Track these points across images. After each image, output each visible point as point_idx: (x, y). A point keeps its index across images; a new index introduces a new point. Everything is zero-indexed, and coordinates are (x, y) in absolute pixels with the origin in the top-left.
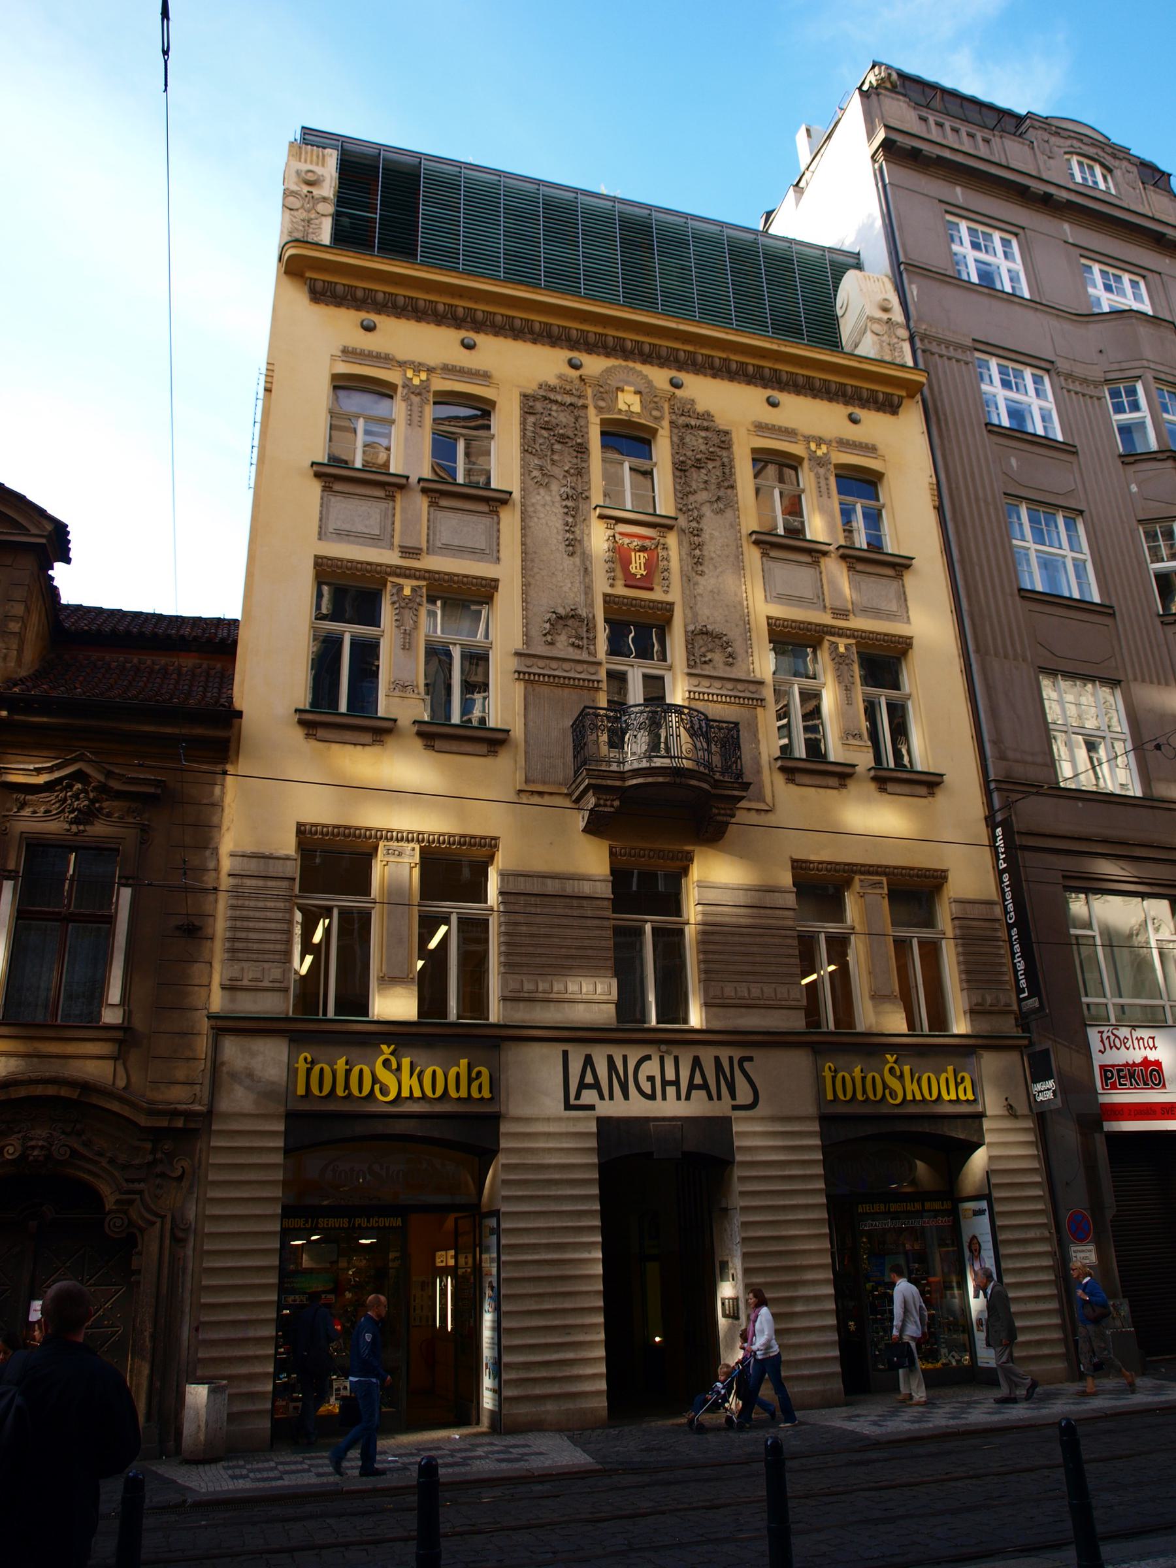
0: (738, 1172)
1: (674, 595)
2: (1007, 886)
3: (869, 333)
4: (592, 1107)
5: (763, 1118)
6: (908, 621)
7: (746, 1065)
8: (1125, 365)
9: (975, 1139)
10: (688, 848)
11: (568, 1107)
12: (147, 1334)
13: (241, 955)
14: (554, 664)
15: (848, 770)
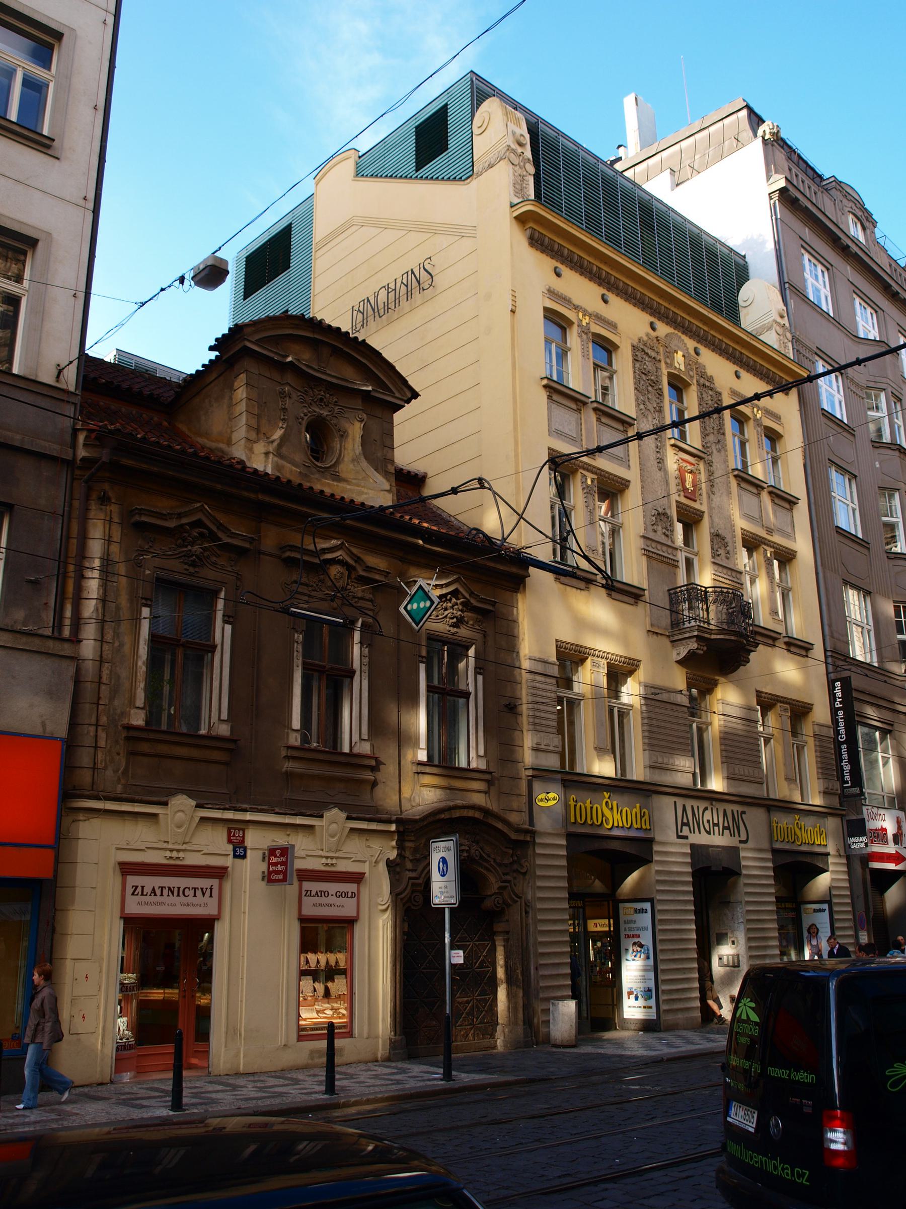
0: (743, 880)
1: (704, 508)
2: (841, 719)
3: (773, 331)
4: (686, 837)
5: (751, 849)
6: (795, 541)
7: (743, 815)
8: (878, 379)
9: (826, 868)
10: (717, 678)
11: (679, 837)
12: (519, 971)
13: (538, 728)
14: (659, 547)
15: (810, 646)
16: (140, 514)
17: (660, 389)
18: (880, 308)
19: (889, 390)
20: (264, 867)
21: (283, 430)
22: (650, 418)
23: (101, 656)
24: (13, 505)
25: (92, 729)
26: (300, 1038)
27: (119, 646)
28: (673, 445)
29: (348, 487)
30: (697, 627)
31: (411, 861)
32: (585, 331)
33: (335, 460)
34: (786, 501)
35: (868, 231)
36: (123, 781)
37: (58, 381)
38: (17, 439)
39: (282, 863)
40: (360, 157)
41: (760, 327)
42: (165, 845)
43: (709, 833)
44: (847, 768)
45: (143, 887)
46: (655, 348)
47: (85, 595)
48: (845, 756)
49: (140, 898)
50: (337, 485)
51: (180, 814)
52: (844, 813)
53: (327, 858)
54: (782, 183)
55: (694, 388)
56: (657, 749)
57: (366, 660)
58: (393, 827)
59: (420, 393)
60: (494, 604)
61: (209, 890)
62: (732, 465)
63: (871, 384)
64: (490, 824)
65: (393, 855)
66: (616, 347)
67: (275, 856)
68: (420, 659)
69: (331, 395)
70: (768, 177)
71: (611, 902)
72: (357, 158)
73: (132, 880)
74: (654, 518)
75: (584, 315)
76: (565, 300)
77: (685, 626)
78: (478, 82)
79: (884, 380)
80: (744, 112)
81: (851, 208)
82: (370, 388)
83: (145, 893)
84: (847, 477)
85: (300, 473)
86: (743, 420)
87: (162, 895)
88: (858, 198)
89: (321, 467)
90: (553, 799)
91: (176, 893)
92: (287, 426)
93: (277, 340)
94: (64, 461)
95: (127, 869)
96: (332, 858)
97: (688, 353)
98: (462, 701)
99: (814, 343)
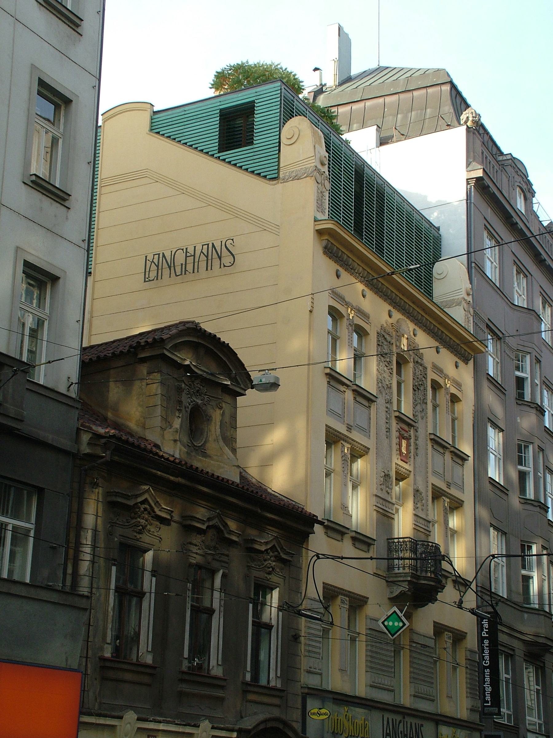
3: (461, 308)
8: (526, 344)
16: (116, 496)
18: (530, 273)
21: (180, 419)
22: (384, 395)
29: (212, 462)
30: (410, 574)
34: (461, 458)
37: (68, 390)
38: (50, 438)
40: (155, 113)
41: (450, 301)
44: (489, 689)
46: (390, 333)
48: (488, 679)
50: (205, 461)
54: (480, 173)
55: (411, 365)
57: (223, 603)
70: (468, 165)
72: (152, 112)
74: (382, 479)
75: (351, 310)
78: (285, 91)
79: (530, 345)
80: (447, 88)
84: (497, 430)
86: (436, 388)
89: (197, 446)
92: (182, 415)
97: (410, 335)
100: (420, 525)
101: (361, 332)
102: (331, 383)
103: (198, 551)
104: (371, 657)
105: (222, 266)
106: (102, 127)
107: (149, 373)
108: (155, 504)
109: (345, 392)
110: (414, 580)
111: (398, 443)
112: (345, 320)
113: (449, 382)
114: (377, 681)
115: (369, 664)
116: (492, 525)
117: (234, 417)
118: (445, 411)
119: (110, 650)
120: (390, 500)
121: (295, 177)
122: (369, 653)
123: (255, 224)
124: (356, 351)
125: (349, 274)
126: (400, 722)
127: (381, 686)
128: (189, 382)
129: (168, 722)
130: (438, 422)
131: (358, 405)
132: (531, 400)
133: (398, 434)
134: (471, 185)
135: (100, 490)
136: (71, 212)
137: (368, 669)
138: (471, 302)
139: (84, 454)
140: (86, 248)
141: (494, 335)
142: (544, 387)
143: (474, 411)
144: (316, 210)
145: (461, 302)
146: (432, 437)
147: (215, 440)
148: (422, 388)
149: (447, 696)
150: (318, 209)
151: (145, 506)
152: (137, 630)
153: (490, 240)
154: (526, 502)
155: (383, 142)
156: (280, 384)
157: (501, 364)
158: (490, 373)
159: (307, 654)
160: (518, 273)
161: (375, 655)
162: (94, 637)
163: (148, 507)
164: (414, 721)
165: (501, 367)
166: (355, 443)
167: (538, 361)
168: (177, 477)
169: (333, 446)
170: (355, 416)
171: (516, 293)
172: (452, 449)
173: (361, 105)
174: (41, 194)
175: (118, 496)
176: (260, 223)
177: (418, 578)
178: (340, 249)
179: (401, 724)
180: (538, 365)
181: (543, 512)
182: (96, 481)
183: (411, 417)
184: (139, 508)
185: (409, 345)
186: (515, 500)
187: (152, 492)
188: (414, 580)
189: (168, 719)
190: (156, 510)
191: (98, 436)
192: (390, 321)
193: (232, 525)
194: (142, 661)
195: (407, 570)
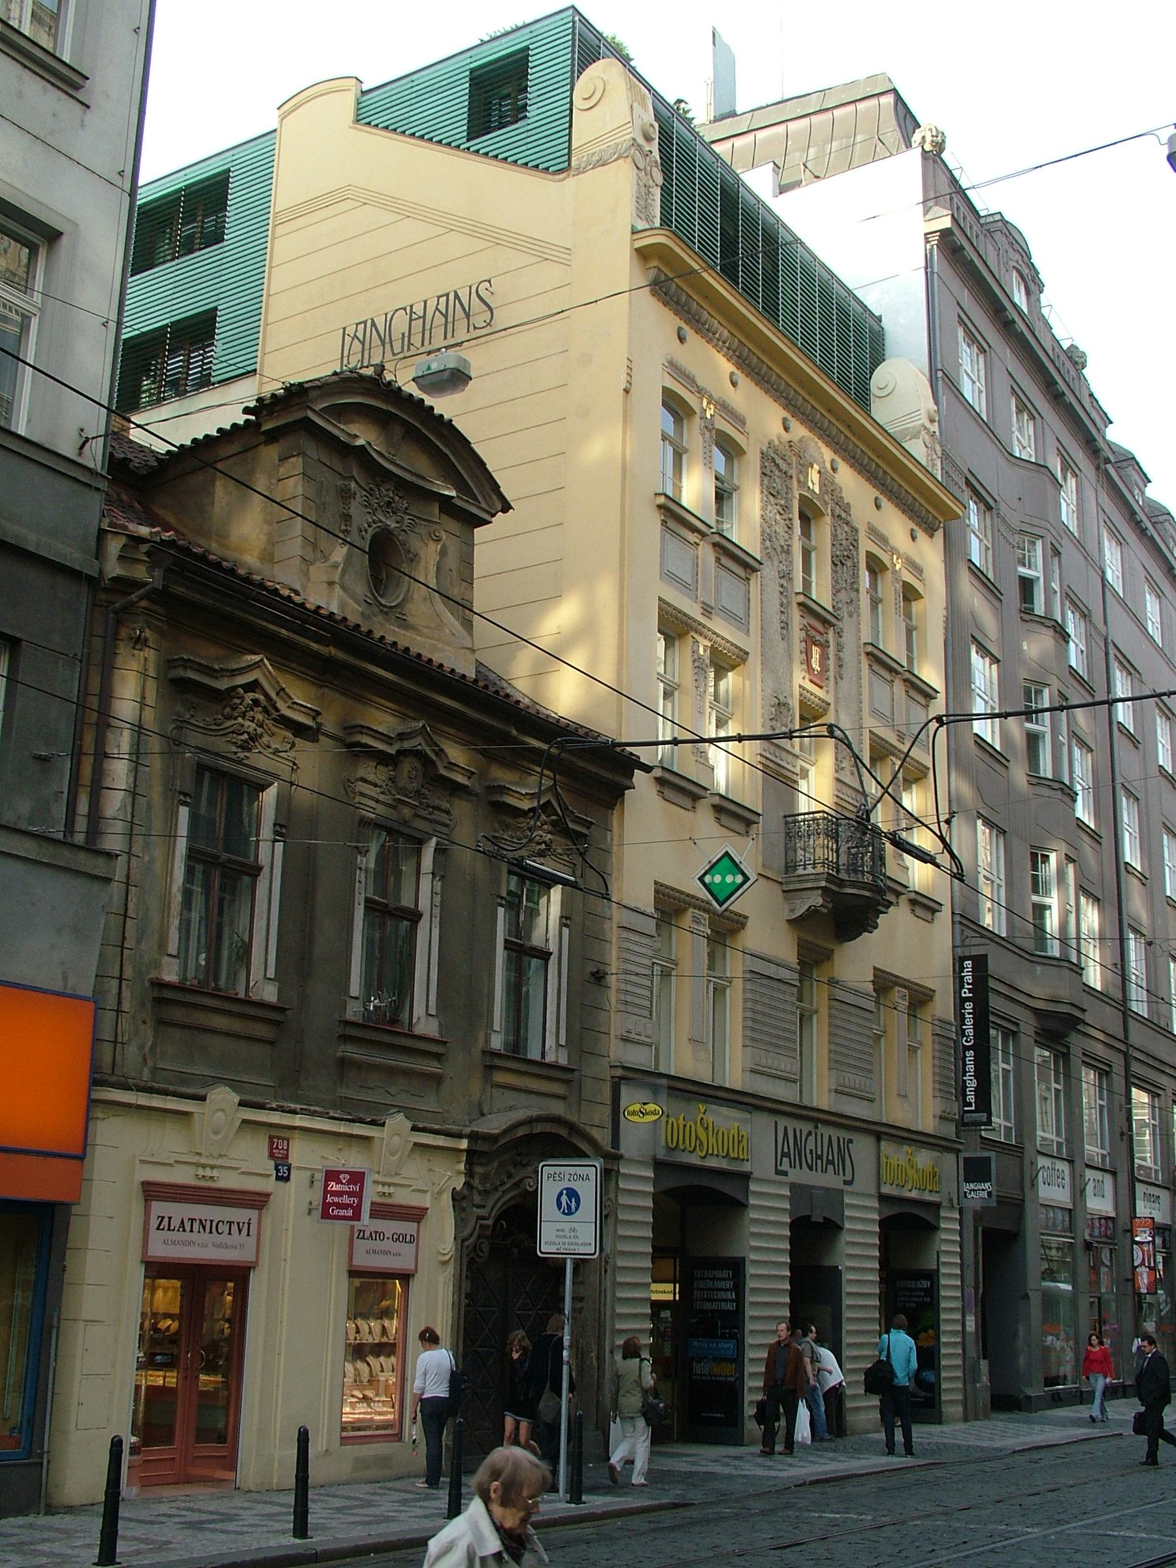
0: (845, 1237)
2: (969, 1013)
3: (920, 442)
4: (785, 1173)
8: (1035, 521)
15: (936, 906)
16: (185, 668)
17: (790, 520)
18: (1039, 414)
19: (1049, 538)
20: (316, 1196)
22: (776, 563)
23: (128, 877)
24: (20, 640)
25: (115, 983)
26: (344, 1441)
27: (149, 861)
28: (800, 604)
29: (419, 638)
31: (480, 1193)
32: (709, 427)
33: (402, 596)
35: (1033, 297)
36: (150, 1063)
37: (80, 454)
38: (33, 541)
39: (351, 1194)
40: (364, 93)
41: (900, 431)
42: (196, 1159)
43: (810, 1168)
44: (972, 1084)
45: (170, 1218)
46: (787, 458)
47: (108, 783)
48: (970, 1067)
49: (165, 1234)
51: (220, 1114)
52: (961, 1147)
53: (384, 1184)
54: (946, 223)
55: (828, 519)
56: (760, 1045)
57: (438, 899)
58: (464, 1144)
59: (512, 504)
60: (589, 825)
61: (246, 1225)
62: (865, 639)
63: (1025, 528)
64: (575, 1145)
65: (459, 1183)
66: (741, 452)
67: (339, 1182)
68: (499, 901)
69: (400, 497)
71: (678, 1260)
72: (359, 93)
73: (159, 1208)
74: (773, 710)
75: (709, 403)
76: (687, 378)
77: (806, 872)
79: (1043, 523)
80: (889, 100)
81: (1017, 262)
82: (453, 493)
83: (172, 1228)
84: (987, 660)
85: (362, 613)
86: (877, 570)
87: (191, 1231)
88: (1025, 248)
89: (385, 606)
90: (654, 1113)
91: (208, 1230)
93: (340, 412)
94: (90, 578)
95: (152, 1192)
96: (389, 1185)
98: (535, 962)
99: (965, 462)
100: (847, 799)
101: (730, 449)
102: (669, 524)
103: (382, 798)
104: (754, 1020)
105: (471, 328)
106: (278, 131)
107: (283, 459)
108: (277, 694)
109: (698, 545)
110: (833, 887)
111: (804, 650)
112: (697, 420)
113: (900, 561)
114: (763, 1062)
115: (749, 1033)
116: (980, 815)
117: (467, 562)
118: (894, 611)
119: (177, 968)
120: (790, 749)
121: (598, 161)
122: (749, 1014)
123: (530, 251)
124: (722, 482)
125: (704, 341)
126: (810, 1133)
127: (774, 1071)
128: (369, 484)
129: (313, 1114)
130: (880, 629)
131: (723, 573)
132: (1045, 613)
133: (803, 634)
134: (933, 243)
135: (150, 654)
136: (90, 116)
137: (748, 1043)
138: (938, 433)
139: (113, 579)
140: (128, 187)
141: (981, 501)
142: (1068, 604)
143: (947, 618)
144: (634, 215)
145: (919, 432)
146: (870, 649)
147: (425, 599)
148: (849, 563)
149: (899, 1095)
150: (640, 214)
151: (257, 695)
152: (246, 938)
153: (969, 346)
154: (1036, 780)
155: (783, 189)
156: (472, 375)
157: (993, 550)
158: (973, 560)
159: (622, 1007)
160: (1019, 411)
161: (759, 1017)
162: (138, 942)
163: (262, 698)
164: (835, 1133)
165: (993, 555)
166: (719, 639)
167: (1057, 553)
168: (328, 646)
169: (677, 643)
170: (717, 591)
171: (1017, 443)
172: (907, 675)
173: (750, 138)
174: (18, 66)
175: (191, 668)
176: (537, 248)
177: (841, 883)
178: (682, 290)
179: (811, 1139)
180: (1056, 560)
181: (1067, 799)
182: (140, 635)
183: (831, 609)
184: (242, 698)
185: (822, 485)
186: (1019, 774)
187: (267, 668)
188: (833, 887)
189: (312, 1108)
190: (280, 704)
191: (139, 540)
192: (786, 437)
193: (456, 753)
194: (254, 996)
195: (819, 869)
